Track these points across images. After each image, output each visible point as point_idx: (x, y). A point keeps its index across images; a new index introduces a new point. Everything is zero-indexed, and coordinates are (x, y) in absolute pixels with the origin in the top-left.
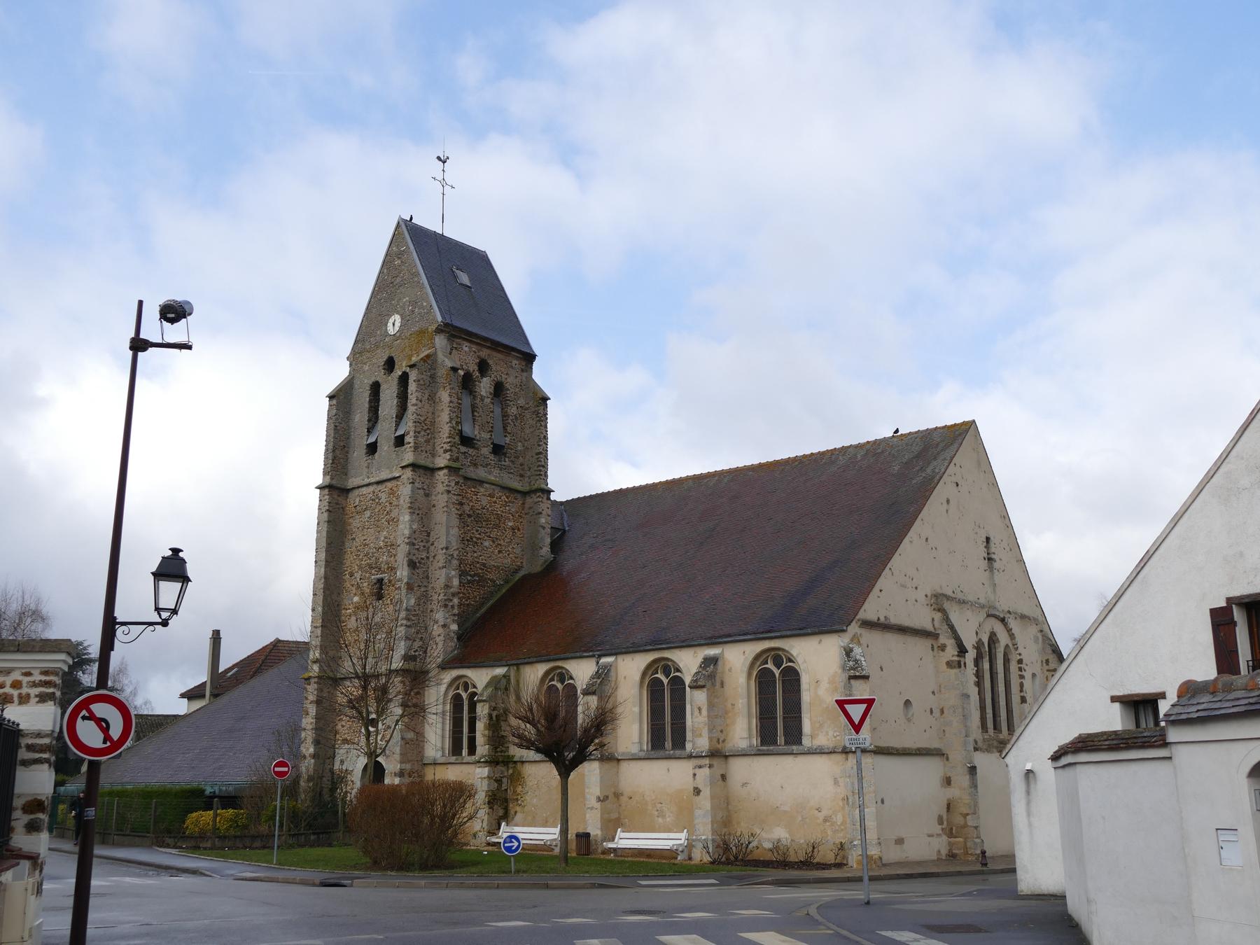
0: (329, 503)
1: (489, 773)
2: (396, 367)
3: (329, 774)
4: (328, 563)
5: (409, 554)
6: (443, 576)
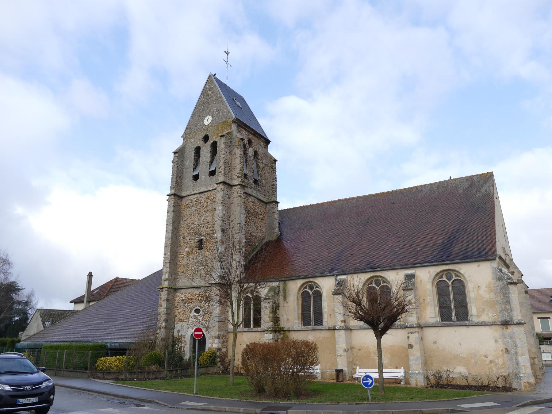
0: (174, 202)
1: (273, 337)
2: (210, 139)
3: (172, 337)
4: (173, 231)
5: (222, 225)
6: (239, 237)
